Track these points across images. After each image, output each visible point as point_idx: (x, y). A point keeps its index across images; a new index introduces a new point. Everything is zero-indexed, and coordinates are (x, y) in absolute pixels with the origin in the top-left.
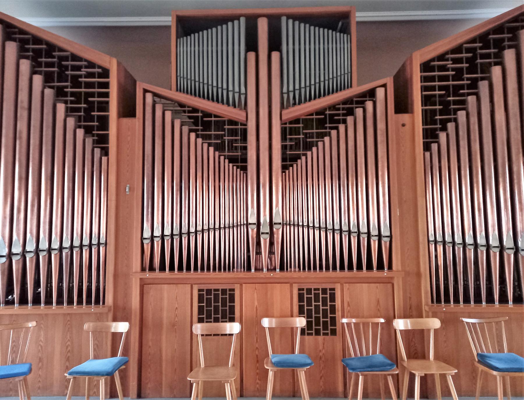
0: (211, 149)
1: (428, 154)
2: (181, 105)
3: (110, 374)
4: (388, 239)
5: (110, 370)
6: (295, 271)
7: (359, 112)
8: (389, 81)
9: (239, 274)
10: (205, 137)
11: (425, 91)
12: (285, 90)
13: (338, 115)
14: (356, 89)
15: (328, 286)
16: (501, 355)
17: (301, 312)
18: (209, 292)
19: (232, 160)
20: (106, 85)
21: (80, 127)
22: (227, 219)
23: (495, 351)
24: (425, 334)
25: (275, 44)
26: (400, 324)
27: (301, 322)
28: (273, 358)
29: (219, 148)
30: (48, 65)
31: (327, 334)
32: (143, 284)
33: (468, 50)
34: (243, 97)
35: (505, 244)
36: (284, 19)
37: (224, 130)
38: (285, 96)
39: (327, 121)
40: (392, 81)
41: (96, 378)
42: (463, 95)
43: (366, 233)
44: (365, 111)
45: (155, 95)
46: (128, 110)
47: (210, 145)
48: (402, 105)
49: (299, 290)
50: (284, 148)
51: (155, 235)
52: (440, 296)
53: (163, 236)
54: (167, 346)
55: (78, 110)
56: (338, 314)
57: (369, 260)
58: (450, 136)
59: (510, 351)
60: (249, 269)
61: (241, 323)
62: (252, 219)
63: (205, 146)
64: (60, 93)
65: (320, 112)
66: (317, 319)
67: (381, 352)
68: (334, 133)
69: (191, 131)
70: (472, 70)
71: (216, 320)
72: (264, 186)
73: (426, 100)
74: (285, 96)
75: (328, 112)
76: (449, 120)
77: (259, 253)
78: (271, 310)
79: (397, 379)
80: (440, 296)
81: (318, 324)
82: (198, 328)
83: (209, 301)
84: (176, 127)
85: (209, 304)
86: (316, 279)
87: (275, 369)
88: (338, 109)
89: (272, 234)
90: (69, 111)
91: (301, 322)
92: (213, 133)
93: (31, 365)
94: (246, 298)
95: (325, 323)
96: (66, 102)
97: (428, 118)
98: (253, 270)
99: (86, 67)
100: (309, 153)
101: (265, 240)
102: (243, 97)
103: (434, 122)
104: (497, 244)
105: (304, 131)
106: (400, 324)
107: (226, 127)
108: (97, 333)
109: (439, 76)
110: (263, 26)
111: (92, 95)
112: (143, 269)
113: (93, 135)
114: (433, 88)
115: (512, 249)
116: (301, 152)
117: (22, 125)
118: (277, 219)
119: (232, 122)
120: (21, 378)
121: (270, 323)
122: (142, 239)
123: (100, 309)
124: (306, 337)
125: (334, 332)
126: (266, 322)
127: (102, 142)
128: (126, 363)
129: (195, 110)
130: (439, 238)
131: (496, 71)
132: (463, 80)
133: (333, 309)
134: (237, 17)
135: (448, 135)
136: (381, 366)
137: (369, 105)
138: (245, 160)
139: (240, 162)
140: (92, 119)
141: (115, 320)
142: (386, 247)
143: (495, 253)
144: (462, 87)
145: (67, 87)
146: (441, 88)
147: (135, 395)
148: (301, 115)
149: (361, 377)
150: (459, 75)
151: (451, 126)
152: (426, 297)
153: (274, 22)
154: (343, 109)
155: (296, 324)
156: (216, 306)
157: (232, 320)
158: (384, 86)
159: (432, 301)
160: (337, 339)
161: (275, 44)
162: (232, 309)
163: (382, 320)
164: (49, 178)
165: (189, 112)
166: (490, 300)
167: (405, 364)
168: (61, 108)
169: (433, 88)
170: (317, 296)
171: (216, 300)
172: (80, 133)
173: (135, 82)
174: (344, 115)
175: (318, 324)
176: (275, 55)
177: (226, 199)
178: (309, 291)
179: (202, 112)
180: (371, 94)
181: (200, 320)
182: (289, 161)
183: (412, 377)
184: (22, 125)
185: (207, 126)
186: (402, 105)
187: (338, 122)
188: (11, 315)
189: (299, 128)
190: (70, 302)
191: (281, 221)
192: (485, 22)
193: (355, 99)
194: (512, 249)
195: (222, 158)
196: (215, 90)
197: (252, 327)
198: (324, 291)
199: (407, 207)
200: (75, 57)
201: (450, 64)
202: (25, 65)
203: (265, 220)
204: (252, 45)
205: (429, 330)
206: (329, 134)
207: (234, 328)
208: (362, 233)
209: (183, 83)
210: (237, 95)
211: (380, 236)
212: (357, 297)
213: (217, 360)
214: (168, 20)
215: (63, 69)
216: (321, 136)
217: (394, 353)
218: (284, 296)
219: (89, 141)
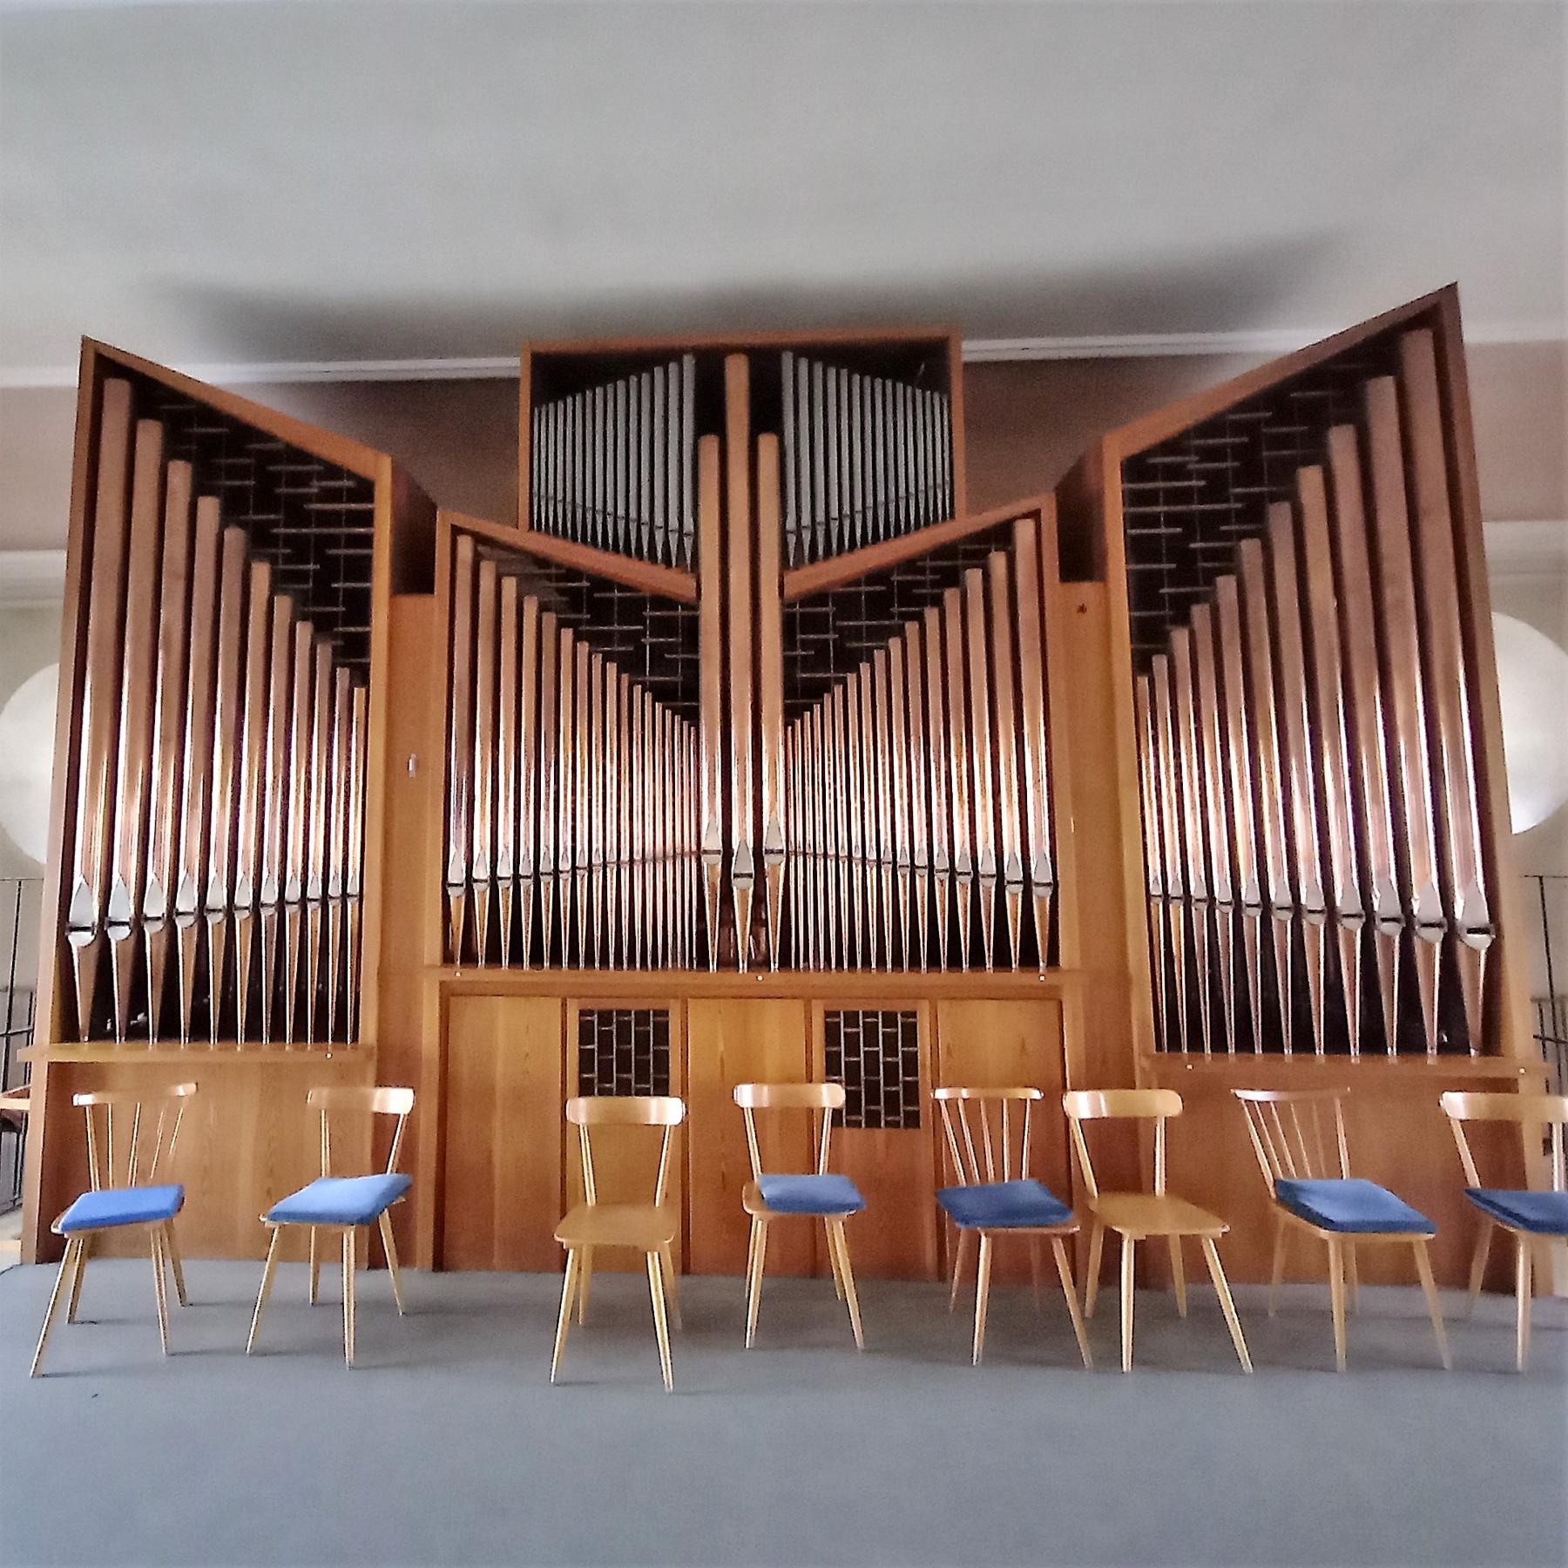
0: (612, 668)
1: (1144, 681)
2: (542, 562)
3: (367, 1223)
4: (1048, 892)
5: (368, 1210)
6: (817, 968)
7: (974, 577)
8: (1047, 504)
9: (680, 977)
10: (596, 640)
11: (1133, 527)
12: (791, 524)
13: (921, 584)
14: (965, 523)
15: (899, 1007)
16: (1334, 1184)
17: (831, 1070)
18: (605, 1017)
19: (662, 694)
20: (367, 518)
21: (304, 618)
22: (648, 837)
23: (1318, 1175)
24: (1142, 1130)
25: (766, 416)
26: (1081, 1105)
27: (832, 1096)
28: (768, 1185)
29: (630, 664)
30: (233, 472)
31: (896, 1125)
32: (448, 995)
33: (1238, 428)
34: (688, 542)
35: (1338, 903)
36: (787, 360)
37: (642, 621)
38: (792, 539)
39: (897, 598)
40: (1054, 505)
41: (334, 1229)
42: (1227, 536)
43: (1048, 885)
44: (987, 578)
45: (479, 539)
46: (415, 575)
47: (607, 658)
48: (1079, 561)
49: (828, 1014)
50: (789, 664)
51: (309, 895)
52: (1180, 1032)
53: (494, 879)
54: (505, 1145)
55: (301, 577)
56: (924, 1076)
57: (998, 939)
58: (1199, 637)
59: (1354, 1172)
60: (703, 963)
61: (684, 1096)
62: (712, 841)
63: (597, 660)
64: (260, 541)
65: (878, 576)
66: (872, 1088)
67: (1031, 1174)
68: (911, 628)
69: (562, 624)
70: (1250, 473)
71: (624, 1090)
72: (741, 760)
73: (1137, 549)
74: (792, 539)
75: (895, 578)
76: (1196, 598)
77: (727, 921)
78: (760, 1064)
79: (1070, 1240)
80: (1180, 1032)
81: (873, 1098)
82: (581, 1110)
83: (605, 1038)
84: (524, 615)
85: (605, 1047)
86: (870, 988)
87: (771, 1215)
88: (922, 571)
89: (760, 875)
90: (279, 583)
91: (832, 1096)
92: (616, 627)
93: (181, 1188)
94: (700, 1035)
95: (892, 1098)
96: (273, 560)
97: (1143, 591)
98: (713, 966)
99: (321, 477)
100: (851, 678)
101: (743, 889)
102: (688, 542)
103: (1158, 602)
104: (1319, 904)
105: (839, 623)
106: (1081, 1105)
107: (648, 613)
108: (340, 1117)
109: (1167, 491)
110: (737, 376)
111: (333, 541)
112: (448, 958)
113: (336, 636)
114: (1153, 521)
115: (1439, 925)
116: (832, 674)
117: (171, 614)
118: (774, 840)
119: (662, 601)
120: (159, 1223)
121: (756, 1096)
122: (65, 925)
123: (346, 1053)
124: (846, 1131)
125: (913, 1120)
126: (746, 1096)
127: (353, 655)
128: (408, 1190)
129: (573, 573)
130: (1175, 889)
131: (1310, 479)
132: (1227, 501)
133: (911, 1063)
134: (675, 355)
135: (1192, 635)
136: (1034, 1214)
137: (998, 561)
138: (692, 690)
139: (681, 699)
140: (331, 597)
141: (381, 1082)
142: (1042, 909)
143: (1315, 924)
144: (1225, 517)
145: (276, 524)
146: (1172, 520)
147: (429, 1263)
148: (834, 583)
149: (984, 1239)
150: (1216, 488)
151: (1199, 613)
152: (1143, 1035)
153: (765, 364)
154: (934, 570)
155: (820, 1100)
156: (624, 1054)
157: (662, 1089)
158: (1035, 515)
159: (1159, 1047)
160: (923, 1135)
161: (766, 416)
162: (662, 1060)
163: (1036, 1095)
164: (231, 736)
165: (559, 578)
166: (1303, 1042)
167: (1093, 1206)
168: (261, 573)
169: (1153, 521)
170: (871, 1031)
171: (623, 1037)
172: (304, 631)
173: (434, 508)
174: (934, 584)
175: (873, 1098)
176: (767, 443)
177: (648, 785)
178: (851, 1019)
179: (590, 578)
180: (1002, 535)
181: (585, 1089)
182: (802, 697)
183: (1113, 1242)
184: (171, 614)
185: (601, 612)
186: (1079, 561)
187: (922, 601)
188: (140, 1066)
189: (827, 614)
190: (277, 1034)
191: (783, 846)
192: (1263, 368)
193: (962, 547)
194: (1439, 925)
195: (638, 689)
196: (621, 525)
197: (713, 1109)
198: (890, 1019)
199: (1095, 807)
200: (298, 455)
201: (1192, 462)
202: (180, 475)
203: (743, 842)
204: (710, 418)
205: (1151, 1121)
206: (901, 632)
207: (667, 1111)
208: (1037, 884)
209: (547, 512)
210: (673, 539)
211: (1027, 881)
212: (974, 1037)
213: (626, 1189)
214: (512, 365)
215: (268, 482)
216: (882, 635)
217: (1064, 1181)
218: (785, 1028)
219: (324, 653)
